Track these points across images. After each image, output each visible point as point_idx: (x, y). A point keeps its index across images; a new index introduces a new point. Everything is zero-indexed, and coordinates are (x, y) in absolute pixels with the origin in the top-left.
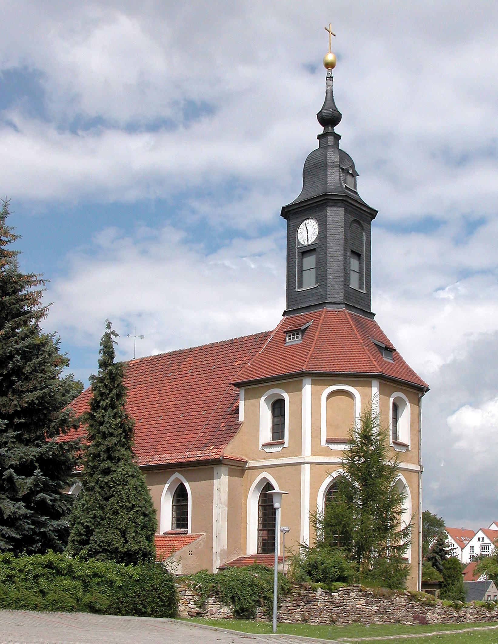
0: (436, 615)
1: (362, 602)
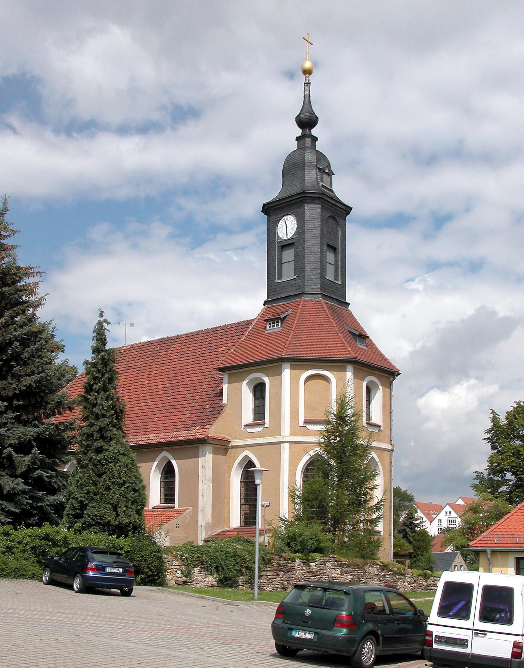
0: (406, 584)
1: (337, 572)
